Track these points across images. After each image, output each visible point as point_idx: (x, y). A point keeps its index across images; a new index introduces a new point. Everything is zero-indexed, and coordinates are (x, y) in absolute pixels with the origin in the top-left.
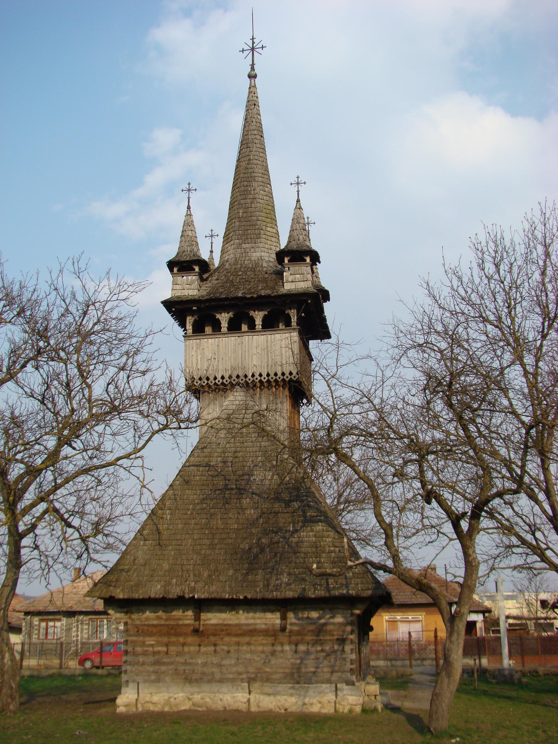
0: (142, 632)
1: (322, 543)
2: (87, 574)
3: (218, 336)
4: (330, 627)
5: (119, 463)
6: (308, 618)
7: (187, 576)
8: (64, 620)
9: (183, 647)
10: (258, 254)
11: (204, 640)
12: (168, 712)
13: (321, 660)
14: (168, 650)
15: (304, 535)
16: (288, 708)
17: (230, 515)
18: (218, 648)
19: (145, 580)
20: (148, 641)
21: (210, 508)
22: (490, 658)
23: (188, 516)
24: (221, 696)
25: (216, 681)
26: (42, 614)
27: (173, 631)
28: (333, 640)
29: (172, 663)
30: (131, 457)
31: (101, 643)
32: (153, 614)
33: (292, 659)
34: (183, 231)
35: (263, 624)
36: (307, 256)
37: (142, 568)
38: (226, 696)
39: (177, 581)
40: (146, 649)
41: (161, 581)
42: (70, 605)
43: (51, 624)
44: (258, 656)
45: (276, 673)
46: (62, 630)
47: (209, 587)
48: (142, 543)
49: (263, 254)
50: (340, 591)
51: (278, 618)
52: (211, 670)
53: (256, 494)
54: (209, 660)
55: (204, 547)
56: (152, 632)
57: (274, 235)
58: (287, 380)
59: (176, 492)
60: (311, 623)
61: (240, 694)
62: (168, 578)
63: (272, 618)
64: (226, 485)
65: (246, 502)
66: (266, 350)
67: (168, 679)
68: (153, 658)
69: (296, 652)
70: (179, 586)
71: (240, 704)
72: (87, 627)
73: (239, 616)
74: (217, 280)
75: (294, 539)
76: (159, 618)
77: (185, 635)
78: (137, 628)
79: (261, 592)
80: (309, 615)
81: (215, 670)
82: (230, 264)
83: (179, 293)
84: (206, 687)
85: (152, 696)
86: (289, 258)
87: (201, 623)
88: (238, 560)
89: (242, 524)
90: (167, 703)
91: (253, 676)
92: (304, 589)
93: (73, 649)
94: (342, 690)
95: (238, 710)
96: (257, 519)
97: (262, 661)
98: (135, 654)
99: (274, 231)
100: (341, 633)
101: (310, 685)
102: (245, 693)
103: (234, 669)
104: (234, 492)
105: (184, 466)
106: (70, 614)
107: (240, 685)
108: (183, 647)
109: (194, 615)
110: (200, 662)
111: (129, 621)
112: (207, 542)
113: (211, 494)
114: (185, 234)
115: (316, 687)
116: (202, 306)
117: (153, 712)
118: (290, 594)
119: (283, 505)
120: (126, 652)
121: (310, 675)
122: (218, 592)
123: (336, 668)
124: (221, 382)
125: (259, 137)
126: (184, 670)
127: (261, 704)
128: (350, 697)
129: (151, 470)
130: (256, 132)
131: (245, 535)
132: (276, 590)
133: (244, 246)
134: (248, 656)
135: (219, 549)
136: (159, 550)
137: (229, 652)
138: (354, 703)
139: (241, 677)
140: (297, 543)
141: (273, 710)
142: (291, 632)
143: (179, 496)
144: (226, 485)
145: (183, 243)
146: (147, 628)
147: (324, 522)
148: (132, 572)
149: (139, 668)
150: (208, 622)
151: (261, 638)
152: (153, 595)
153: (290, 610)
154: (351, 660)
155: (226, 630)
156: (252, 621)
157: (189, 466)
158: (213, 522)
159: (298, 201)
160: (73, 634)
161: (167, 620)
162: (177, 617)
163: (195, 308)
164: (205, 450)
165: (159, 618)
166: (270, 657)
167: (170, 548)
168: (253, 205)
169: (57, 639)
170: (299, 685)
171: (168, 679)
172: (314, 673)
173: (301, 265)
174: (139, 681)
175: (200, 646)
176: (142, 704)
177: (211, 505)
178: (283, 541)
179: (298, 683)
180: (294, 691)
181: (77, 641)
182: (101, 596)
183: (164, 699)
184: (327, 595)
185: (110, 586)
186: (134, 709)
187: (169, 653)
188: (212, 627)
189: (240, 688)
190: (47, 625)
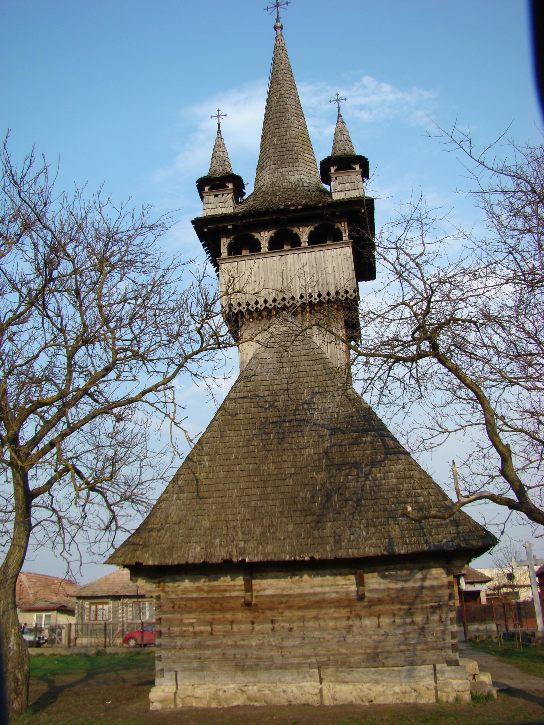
0: (179, 608)
5: (144, 398)
7: (234, 534)
8: (111, 603)
9: (232, 625)
10: (297, 177)
11: (258, 616)
14: (212, 630)
15: (380, 477)
16: (373, 699)
17: (285, 458)
18: (276, 625)
20: (187, 619)
21: (258, 451)
23: (232, 461)
24: (284, 687)
27: (218, 606)
30: (159, 388)
31: (142, 623)
33: (373, 635)
34: (213, 153)
36: (356, 164)
37: (176, 527)
38: (290, 686)
39: (221, 541)
40: (184, 629)
41: (200, 542)
43: (100, 607)
44: (329, 634)
45: (354, 654)
46: (109, 612)
47: (263, 547)
48: (175, 496)
49: (302, 176)
51: (352, 585)
52: (269, 654)
54: (266, 641)
55: (254, 498)
56: (191, 607)
57: (312, 161)
58: (343, 299)
61: (309, 684)
63: (345, 585)
67: (214, 666)
68: (195, 640)
69: (379, 626)
70: (224, 547)
71: (310, 696)
74: (254, 200)
77: (233, 610)
78: (173, 602)
79: (332, 550)
82: (266, 187)
83: (210, 213)
84: (263, 676)
85: (194, 688)
86: (335, 168)
87: (254, 594)
90: (215, 697)
91: (325, 659)
94: (443, 672)
95: (308, 705)
97: (336, 640)
98: (171, 635)
99: (312, 157)
102: (314, 681)
103: (300, 652)
106: (116, 598)
107: (308, 672)
108: (232, 625)
109: (245, 585)
110: (254, 644)
111: (162, 595)
112: (258, 492)
114: (216, 155)
116: (239, 223)
117: (197, 709)
118: (371, 551)
120: (160, 634)
122: (275, 554)
124: (263, 306)
125: (289, 76)
127: (337, 696)
128: (454, 682)
129: (183, 408)
130: (285, 71)
133: (280, 170)
134: (317, 634)
137: (291, 630)
138: (461, 688)
139: (309, 661)
141: (354, 702)
142: (370, 600)
146: (185, 603)
149: (177, 654)
150: (262, 593)
151: (333, 610)
152: (191, 560)
154: (452, 632)
155: (286, 602)
156: (319, 590)
161: (209, 592)
162: (221, 588)
167: (210, 501)
168: (288, 133)
171: (214, 666)
173: (351, 174)
174: (176, 669)
175: (253, 623)
176: (182, 699)
181: (123, 621)
182: (125, 563)
183: (210, 693)
186: (172, 706)
187: (214, 633)
188: (268, 599)
189: (307, 676)
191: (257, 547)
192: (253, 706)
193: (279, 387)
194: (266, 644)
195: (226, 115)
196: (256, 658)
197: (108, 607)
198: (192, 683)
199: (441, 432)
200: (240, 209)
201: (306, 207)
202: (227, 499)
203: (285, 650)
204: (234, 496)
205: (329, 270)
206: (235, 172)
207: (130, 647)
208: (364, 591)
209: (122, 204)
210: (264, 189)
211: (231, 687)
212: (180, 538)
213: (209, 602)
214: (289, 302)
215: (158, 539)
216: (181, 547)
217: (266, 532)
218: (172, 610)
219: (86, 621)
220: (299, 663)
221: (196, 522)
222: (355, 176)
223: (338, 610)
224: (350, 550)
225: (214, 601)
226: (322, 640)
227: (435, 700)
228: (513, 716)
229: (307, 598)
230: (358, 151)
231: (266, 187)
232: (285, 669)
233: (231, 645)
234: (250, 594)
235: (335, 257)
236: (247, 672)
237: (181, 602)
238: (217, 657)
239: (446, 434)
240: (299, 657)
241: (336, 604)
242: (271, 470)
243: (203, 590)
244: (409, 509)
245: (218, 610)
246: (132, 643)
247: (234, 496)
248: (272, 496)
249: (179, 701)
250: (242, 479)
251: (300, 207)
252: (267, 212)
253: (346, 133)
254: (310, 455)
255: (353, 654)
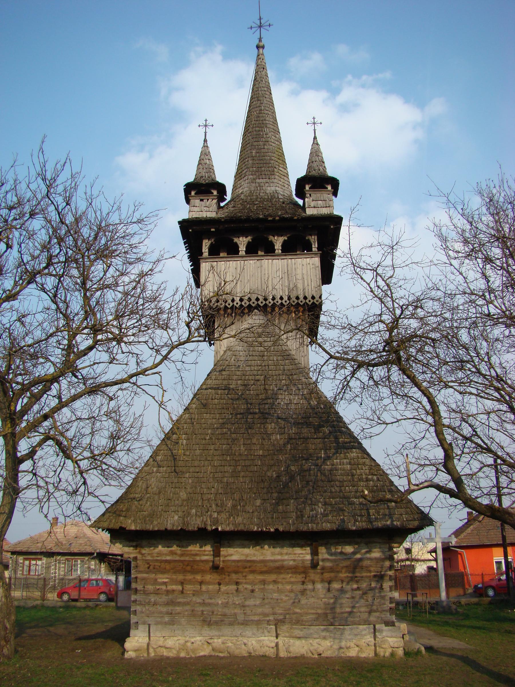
0: (154, 568)
1: (358, 471)
2: (82, 509)
3: (236, 259)
4: (366, 563)
6: (341, 553)
8: (45, 560)
9: (200, 585)
10: (273, 189)
11: (225, 578)
12: (184, 658)
13: (357, 599)
14: (183, 589)
15: (337, 462)
17: (254, 441)
18: (240, 587)
19: (160, 510)
20: (160, 578)
21: (231, 433)
22: (401, 592)
23: (207, 441)
24: (245, 641)
25: (239, 623)
26: (28, 554)
27: (189, 568)
28: (370, 577)
29: (188, 604)
30: (146, 373)
32: (166, 549)
33: (324, 598)
34: (200, 160)
35: (292, 560)
36: (328, 184)
37: (156, 497)
38: (250, 639)
39: (196, 512)
40: (158, 587)
41: (178, 511)
42: (50, 547)
43: (33, 562)
44: (286, 596)
47: (234, 518)
49: (277, 188)
50: (384, 523)
51: (308, 554)
52: (233, 612)
53: (282, 419)
54: (230, 600)
56: (165, 568)
57: (285, 175)
59: (193, 416)
60: (345, 559)
61: (266, 638)
62: (186, 508)
63: (302, 554)
64: (249, 409)
65: (270, 427)
66: (286, 274)
69: (329, 590)
71: (268, 648)
72: (63, 565)
73: (265, 551)
74: (234, 207)
75: (326, 467)
76: (172, 553)
77: (203, 572)
79: (294, 524)
80: (343, 550)
81: (237, 611)
82: (245, 196)
83: (195, 215)
84: (227, 630)
85: (166, 640)
86: (310, 186)
88: (265, 489)
89: (268, 450)
90: (183, 647)
91: (281, 617)
92: (343, 521)
93: (51, 583)
94: (381, 631)
95: (265, 656)
96: (284, 444)
97: (292, 601)
98: (146, 593)
100: (380, 569)
101: (346, 627)
102: (271, 636)
103: (260, 610)
104: (257, 416)
105: (200, 389)
106: (50, 554)
109: (213, 551)
110: (220, 602)
111: (139, 556)
112: (230, 469)
113: (231, 418)
114: (202, 162)
115: (351, 629)
117: (168, 658)
118: (327, 526)
119: (313, 431)
121: (346, 615)
123: (375, 608)
124: (239, 304)
126: (202, 611)
127: (291, 649)
128: (390, 640)
130: (265, 89)
131: (272, 462)
132: (312, 522)
133: (258, 181)
134: (275, 595)
135: (243, 477)
136: (175, 477)
137: (253, 591)
139: (268, 618)
140: (331, 470)
142: (323, 568)
143: (196, 420)
144: (249, 409)
145: (201, 170)
146: (159, 564)
147: (358, 448)
148: (145, 500)
149: (151, 609)
151: (290, 575)
152: (169, 527)
153: (321, 545)
155: (250, 567)
156: (279, 557)
157: (206, 389)
158: (235, 448)
159: (315, 138)
160: (52, 571)
161: (182, 555)
162: (193, 552)
163: (213, 230)
164: (224, 373)
165: (172, 553)
166: (300, 597)
167: (187, 475)
169: (38, 575)
170: (332, 627)
171: (183, 621)
172: (350, 613)
173: (323, 192)
174: (150, 623)
175: (219, 584)
177: (232, 430)
178: (314, 469)
179: (332, 625)
180: (328, 634)
181: (55, 577)
183: (179, 644)
184: (370, 526)
185: (120, 516)
187: (185, 592)
188: (233, 564)
189: (266, 631)
190: (30, 563)
191: (229, 518)
192: (217, 656)
193: (250, 377)
194: (231, 603)
195: (212, 126)
196: (221, 615)
197: (41, 563)
198: (163, 635)
199: (380, 424)
200: (222, 215)
201: (283, 219)
202: (202, 474)
203: (247, 608)
204: (209, 472)
205: (299, 277)
206: (220, 181)
207: (63, 601)
208: (318, 560)
209: (115, 199)
210: (242, 197)
211: (198, 639)
212: (160, 507)
213: (181, 564)
214: (262, 303)
215: (140, 507)
216: (161, 515)
217: (237, 506)
218: (147, 570)
219: (19, 575)
220: (259, 620)
221: (174, 494)
222: (326, 194)
223: (294, 576)
224: (310, 525)
225: (186, 564)
226: (279, 601)
227: (374, 655)
228: (441, 668)
229: (268, 564)
230: (330, 173)
231: (245, 196)
232: (247, 625)
233: (200, 603)
234: (219, 558)
235: (305, 265)
236: (213, 627)
237: (156, 564)
238: (186, 613)
239: (384, 426)
240: (260, 615)
241: (293, 570)
242: (242, 451)
243: (176, 554)
244: (366, 492)
245: (189, 572)
246: (66, 597)
247: (209, 472)
248: (242, 474)
249: (151, 650)
250: (216, 457)
251: (277, 218)
252: (248, 220)
253: (320, 155)
254: (276, 439)
255: (306, 614)
